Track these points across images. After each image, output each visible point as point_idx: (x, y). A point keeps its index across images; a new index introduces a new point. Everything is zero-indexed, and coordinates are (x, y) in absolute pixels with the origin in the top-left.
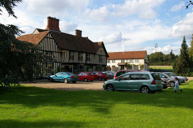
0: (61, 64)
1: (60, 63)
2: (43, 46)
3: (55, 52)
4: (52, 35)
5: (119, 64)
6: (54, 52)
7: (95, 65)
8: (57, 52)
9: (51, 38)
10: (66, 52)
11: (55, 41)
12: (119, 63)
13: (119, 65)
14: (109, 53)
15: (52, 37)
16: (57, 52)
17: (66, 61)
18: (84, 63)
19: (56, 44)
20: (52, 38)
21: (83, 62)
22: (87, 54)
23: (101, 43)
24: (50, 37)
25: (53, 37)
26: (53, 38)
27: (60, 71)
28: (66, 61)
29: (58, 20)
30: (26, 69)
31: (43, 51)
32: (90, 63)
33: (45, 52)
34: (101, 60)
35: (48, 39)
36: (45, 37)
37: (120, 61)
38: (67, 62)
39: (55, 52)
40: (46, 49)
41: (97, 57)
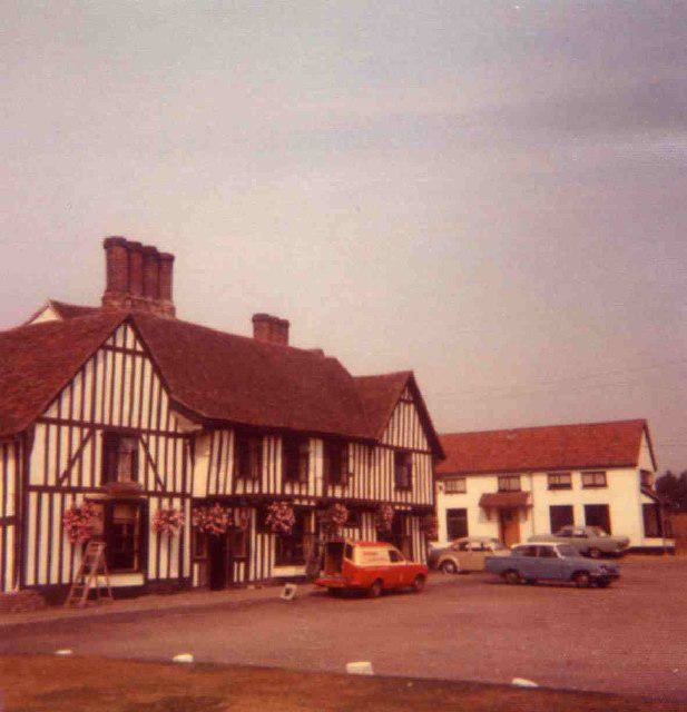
0: (188, 502)
2: (406, 434)
3: (158, 433)
4: (138, 337)
6: (149, 432)
8: (168, 435)
9: (134, 353)
14: (449, 437)
15: (139, 348)
16: (168, 435)
18: (315, 498)
19: (163, 385)
21: (311, 493)
23: (407, 377)
24: (130, 345)
25: (143, 345)
26: (146, 354)
29: (170, 259)
32: (348, 494)
37: (490, 485)
38: (221, 492)
39: (158, 433)
40: (361, 492)
41: (386, 461)
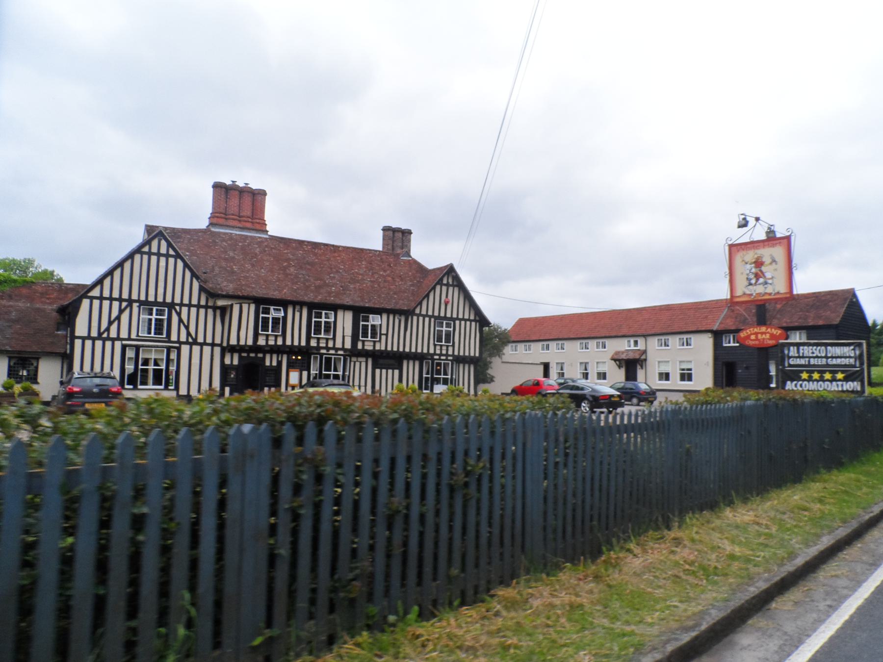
1: (213, 345)
4: (170, 245)
5: (616, 357)
7: (420, 357)
10: (236, 308)
11: (186, 265)
12: (617, 353)
13: (619, 360)
15: (171, 252)
17: (458, 315)
19: (194, 275)
20: (172, 256)
22: (360, 312)
26: (178, 256)
27: (10, 378)
28: (458, 315)
30: (28, 375)
31: (124, 304)
33: (135, 305)
34: (447, 340)
35: (154, 259)
36: (138, 250)
